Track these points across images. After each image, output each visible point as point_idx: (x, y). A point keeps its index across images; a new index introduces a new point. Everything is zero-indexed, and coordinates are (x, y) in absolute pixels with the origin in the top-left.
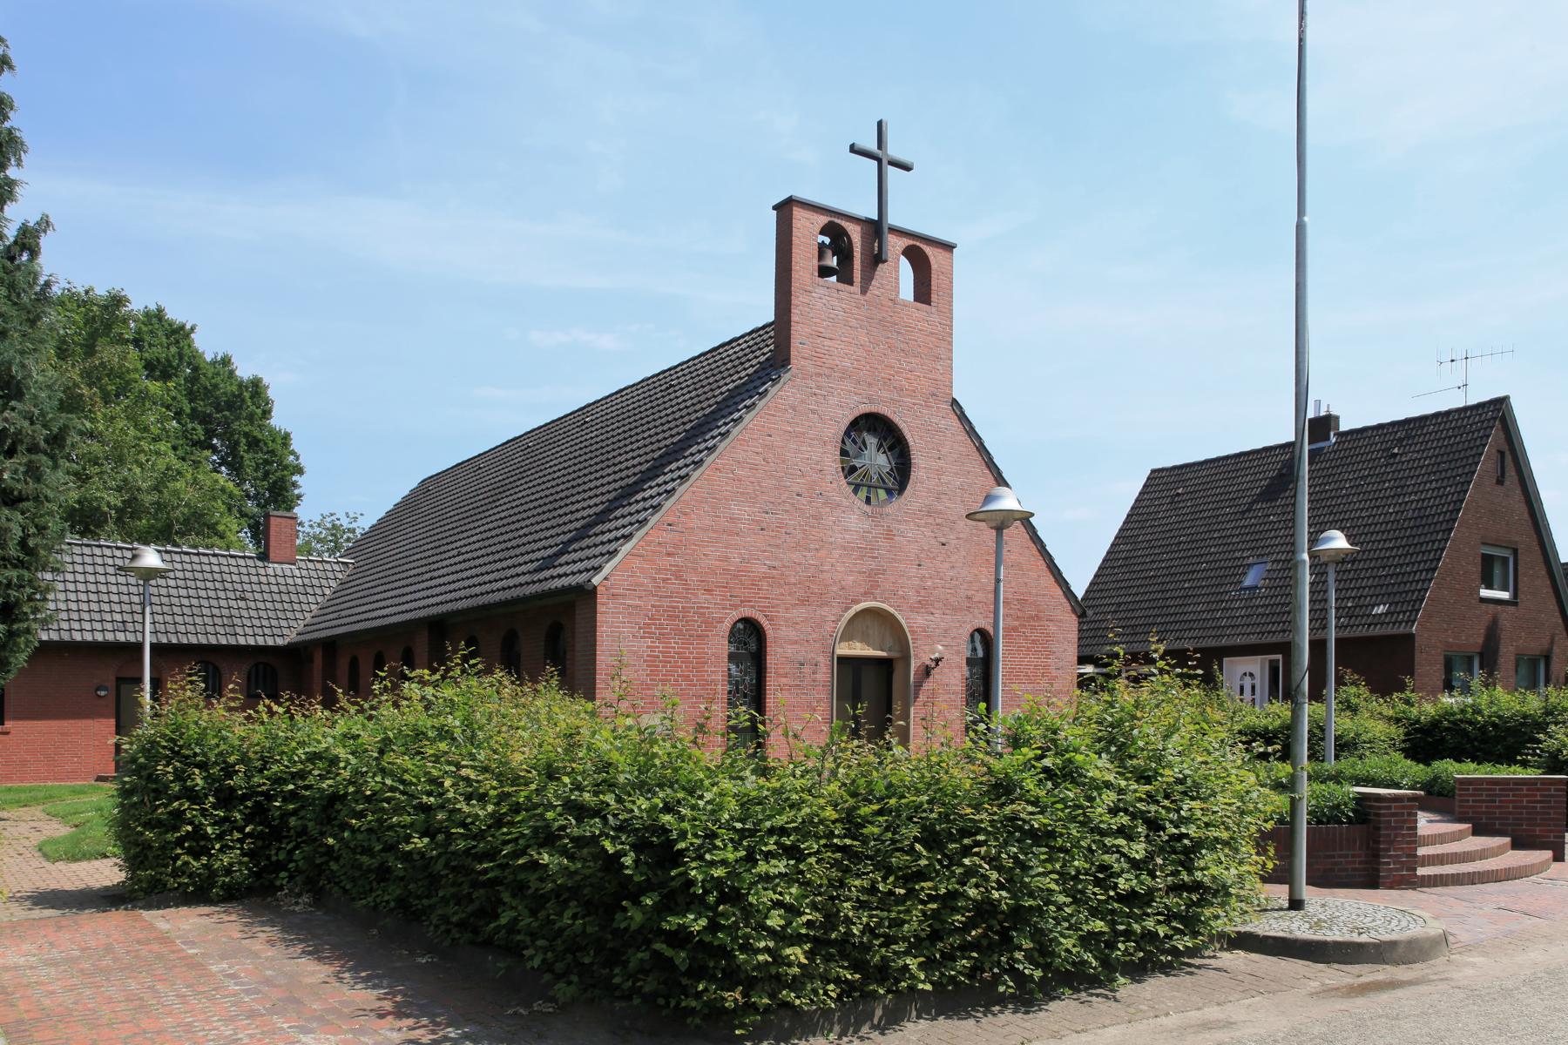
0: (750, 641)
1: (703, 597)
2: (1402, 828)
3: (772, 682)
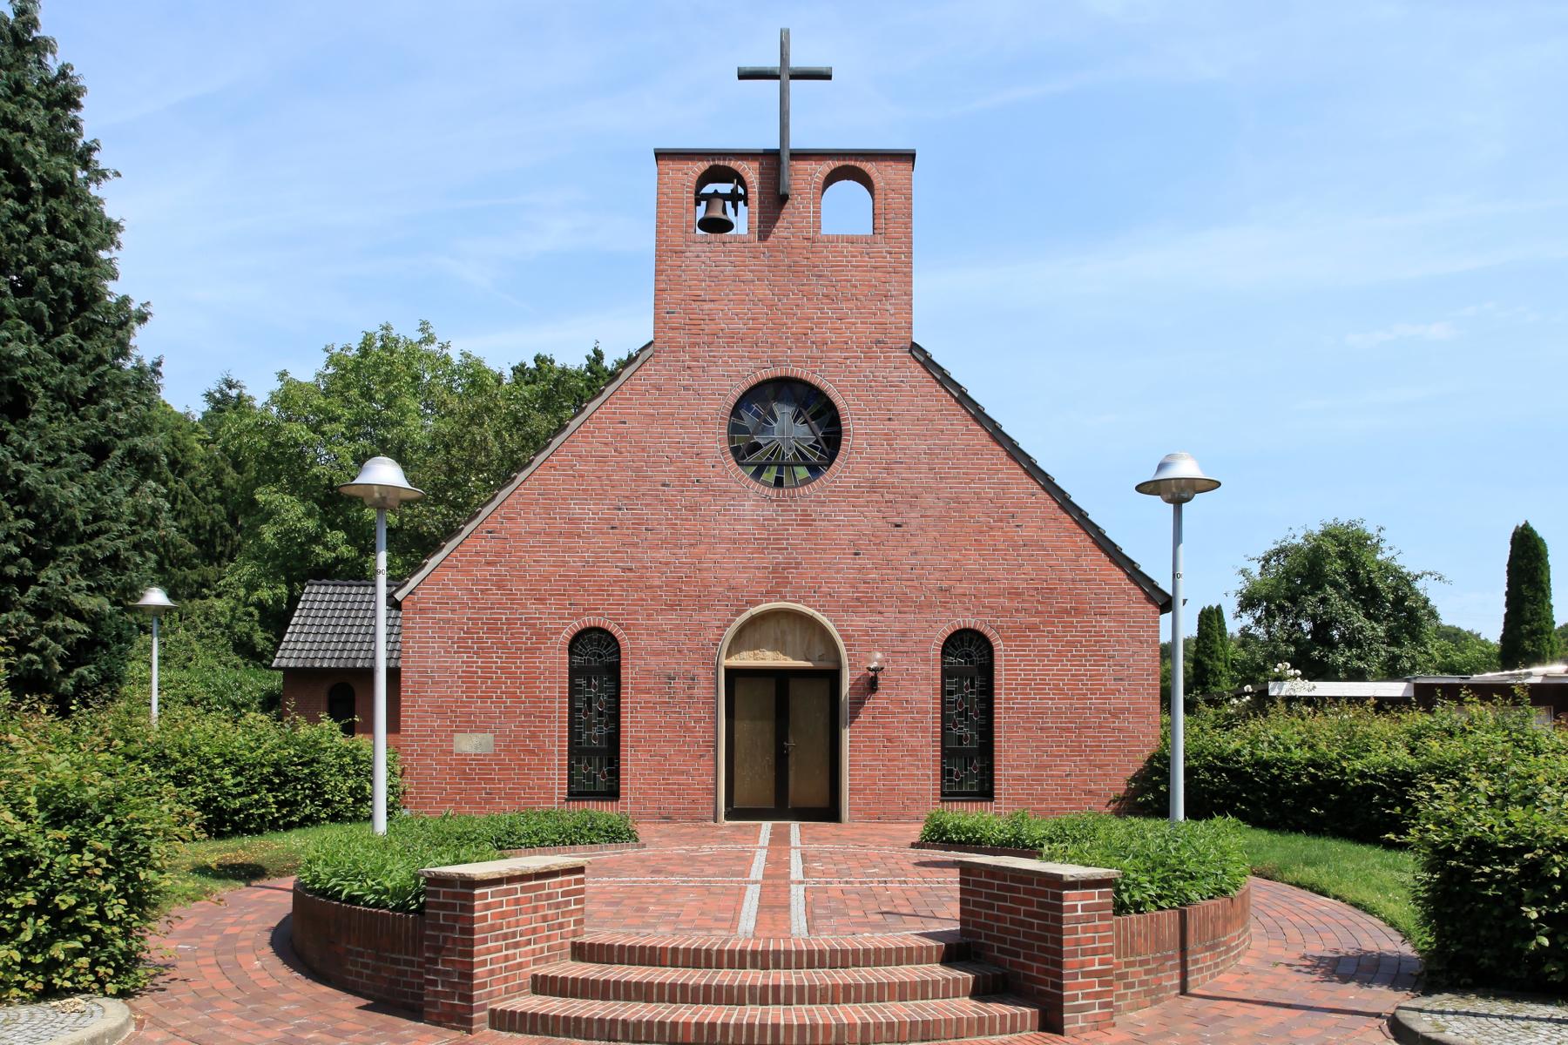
0: (596, 658)
1: (532, 607)
2: (452, 929)
3: (628, 700)
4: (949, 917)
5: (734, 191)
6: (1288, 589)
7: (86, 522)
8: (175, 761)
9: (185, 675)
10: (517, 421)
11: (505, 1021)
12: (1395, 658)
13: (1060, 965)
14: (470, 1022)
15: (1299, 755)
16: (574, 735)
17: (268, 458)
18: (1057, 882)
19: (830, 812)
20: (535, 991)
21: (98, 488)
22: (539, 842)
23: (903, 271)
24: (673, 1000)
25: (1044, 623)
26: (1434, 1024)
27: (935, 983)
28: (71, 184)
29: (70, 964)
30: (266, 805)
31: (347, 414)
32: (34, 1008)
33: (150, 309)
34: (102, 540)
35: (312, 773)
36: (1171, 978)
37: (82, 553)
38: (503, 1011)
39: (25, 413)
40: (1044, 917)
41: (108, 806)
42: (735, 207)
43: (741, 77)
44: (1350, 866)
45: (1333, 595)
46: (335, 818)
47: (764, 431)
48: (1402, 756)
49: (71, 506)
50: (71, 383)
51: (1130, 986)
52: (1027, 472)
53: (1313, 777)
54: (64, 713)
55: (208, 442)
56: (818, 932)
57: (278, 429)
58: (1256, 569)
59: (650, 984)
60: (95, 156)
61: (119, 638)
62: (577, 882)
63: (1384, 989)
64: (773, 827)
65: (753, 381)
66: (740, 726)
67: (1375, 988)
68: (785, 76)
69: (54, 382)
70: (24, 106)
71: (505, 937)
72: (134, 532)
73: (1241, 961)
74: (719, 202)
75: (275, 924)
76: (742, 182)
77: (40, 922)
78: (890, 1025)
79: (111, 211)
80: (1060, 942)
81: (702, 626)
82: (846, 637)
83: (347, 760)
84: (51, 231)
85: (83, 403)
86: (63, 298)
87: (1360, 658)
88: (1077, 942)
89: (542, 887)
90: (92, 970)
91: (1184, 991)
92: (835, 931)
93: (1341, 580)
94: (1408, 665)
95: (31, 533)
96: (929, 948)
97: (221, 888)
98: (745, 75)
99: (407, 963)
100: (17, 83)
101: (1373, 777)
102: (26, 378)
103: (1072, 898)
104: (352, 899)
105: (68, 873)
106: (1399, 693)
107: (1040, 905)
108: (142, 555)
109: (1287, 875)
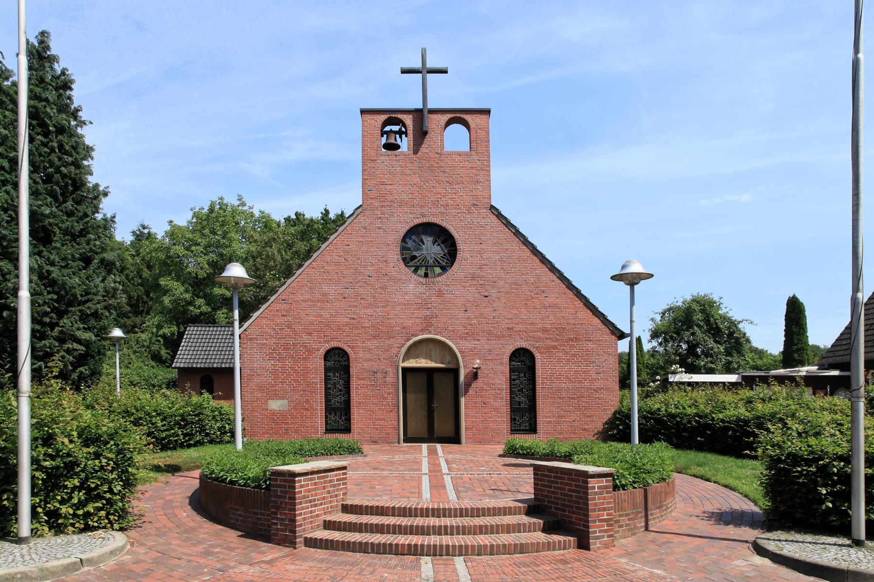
0: (338, 363)
1: (305, 337)
2: (285, 497)
4: (528, 491)
5: (400, 129)
6: (675, 328)
7: (82, 296)
8: (133, 414)
9: (129, 371)
10: (288, 245)
11: (312, 543)
12: (730, 363)
13: (587, 516)
14: (295, 543)
15: (689, 411)
16: (327, 401)
17: (164, 263)
18: (585, 475)
19: (455, 439)
20: (325, 528)
21: (87, 278)
22: (316, 454)
23: (486, 169)
24: (394, 533)
25: (561, 345)
26: (777, 546)
27: (524, 525)
28: (69, 127)
29: (96, 514)
30: (177, 435)
31: (204, 242)
32: (80, 536)
33: (109, 190)
34: (90, 304)
35: (199, 420)
36: (640, 522)
37: (80, 311)
38: (311, 538)
39: (50, 242)
40: (578, 492)
41: (112, 436)
42: (401, 137)
43: (402, 72)
44: (720, 467)
45: (698, 332)
46: (211, 442)
47: (418, 249)
48: (743, 412)
49: (74, 288)
50: (72, 227)
51: (621, 526)
52: (550, 270)
53: (696, 421)
54: (78, 389)
55: (134, 256)
56: (463, 499)
57: (168, 249)
58: (658, 318)
59: (383, 525)
60: (80, 114)
61: (99, 353)
62: (343, 474)
63: (747, 528)
64: (428, 446)
65: (412, 225)
66: (410, 396)
67: (743, 528)
68: (424, 72)
69: (64, 226)
70: (45, 89)
71: (310, 501)
72: (105, 300)
73: (673, 514)
74: (393, 135)
75: (190, 495)
76: (404, 125)
77: (81, 494)
78: (504, 545)
79: (88, 141)
80: (587, 505)
81: (390, 347)
82: (461, 352)
83: (217, 413)
84: (60, 151)
85: (78, 237)
86: (67, 184)
87: (712, 363)
88: (596, 504)
89: (327, 476)
90: (107, 518)
91: (647, 529)
92: (471, 499)
93: (702, 324)
94: (736, 366)
95: (55, 301)
96: (520, 507)
97: (162, 477)
98: (404, 71)
99: (262, 514)
100: (41, 77)
101: (728, 422)
102: (50, 224)
103: (593, 483)
104: (232, 482)
105: (94, 469)
106: (734, 380)
107: (576, 486)
108: (109, 312)
109: (689, 471)
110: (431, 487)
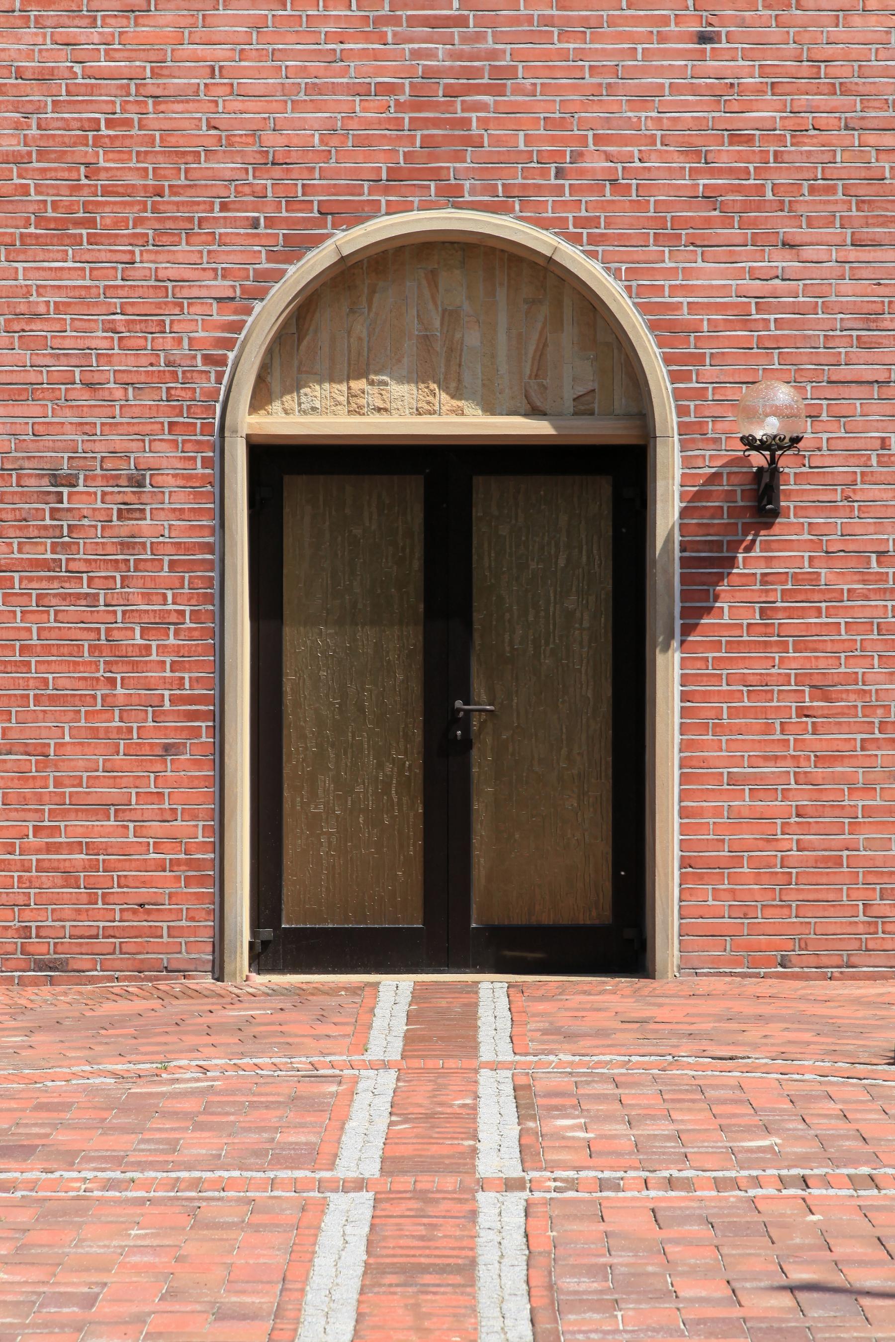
19: (617, 943)
64: (419, 995)
66: (297, 641)
81: (170, 294)
82: (666, 330)
110: (374, 1272)
